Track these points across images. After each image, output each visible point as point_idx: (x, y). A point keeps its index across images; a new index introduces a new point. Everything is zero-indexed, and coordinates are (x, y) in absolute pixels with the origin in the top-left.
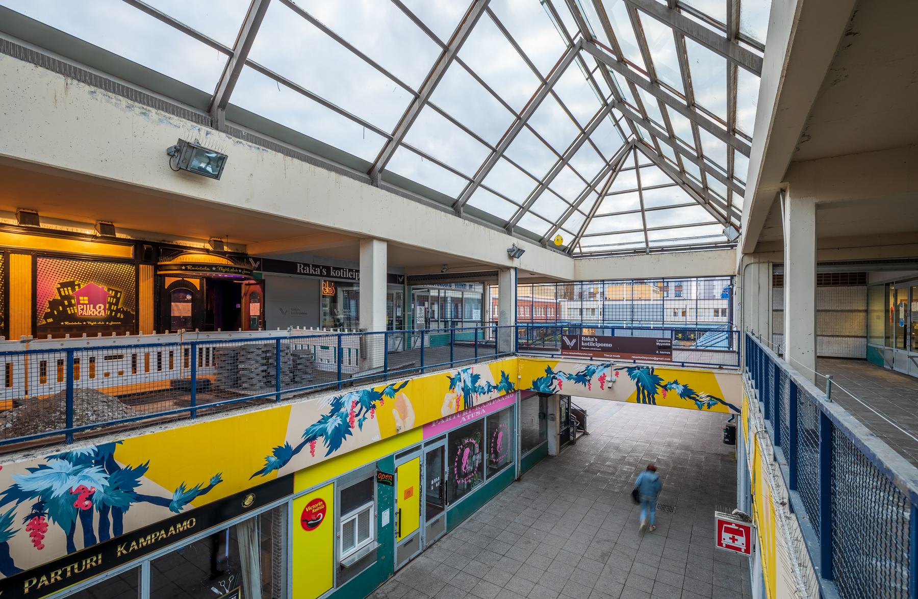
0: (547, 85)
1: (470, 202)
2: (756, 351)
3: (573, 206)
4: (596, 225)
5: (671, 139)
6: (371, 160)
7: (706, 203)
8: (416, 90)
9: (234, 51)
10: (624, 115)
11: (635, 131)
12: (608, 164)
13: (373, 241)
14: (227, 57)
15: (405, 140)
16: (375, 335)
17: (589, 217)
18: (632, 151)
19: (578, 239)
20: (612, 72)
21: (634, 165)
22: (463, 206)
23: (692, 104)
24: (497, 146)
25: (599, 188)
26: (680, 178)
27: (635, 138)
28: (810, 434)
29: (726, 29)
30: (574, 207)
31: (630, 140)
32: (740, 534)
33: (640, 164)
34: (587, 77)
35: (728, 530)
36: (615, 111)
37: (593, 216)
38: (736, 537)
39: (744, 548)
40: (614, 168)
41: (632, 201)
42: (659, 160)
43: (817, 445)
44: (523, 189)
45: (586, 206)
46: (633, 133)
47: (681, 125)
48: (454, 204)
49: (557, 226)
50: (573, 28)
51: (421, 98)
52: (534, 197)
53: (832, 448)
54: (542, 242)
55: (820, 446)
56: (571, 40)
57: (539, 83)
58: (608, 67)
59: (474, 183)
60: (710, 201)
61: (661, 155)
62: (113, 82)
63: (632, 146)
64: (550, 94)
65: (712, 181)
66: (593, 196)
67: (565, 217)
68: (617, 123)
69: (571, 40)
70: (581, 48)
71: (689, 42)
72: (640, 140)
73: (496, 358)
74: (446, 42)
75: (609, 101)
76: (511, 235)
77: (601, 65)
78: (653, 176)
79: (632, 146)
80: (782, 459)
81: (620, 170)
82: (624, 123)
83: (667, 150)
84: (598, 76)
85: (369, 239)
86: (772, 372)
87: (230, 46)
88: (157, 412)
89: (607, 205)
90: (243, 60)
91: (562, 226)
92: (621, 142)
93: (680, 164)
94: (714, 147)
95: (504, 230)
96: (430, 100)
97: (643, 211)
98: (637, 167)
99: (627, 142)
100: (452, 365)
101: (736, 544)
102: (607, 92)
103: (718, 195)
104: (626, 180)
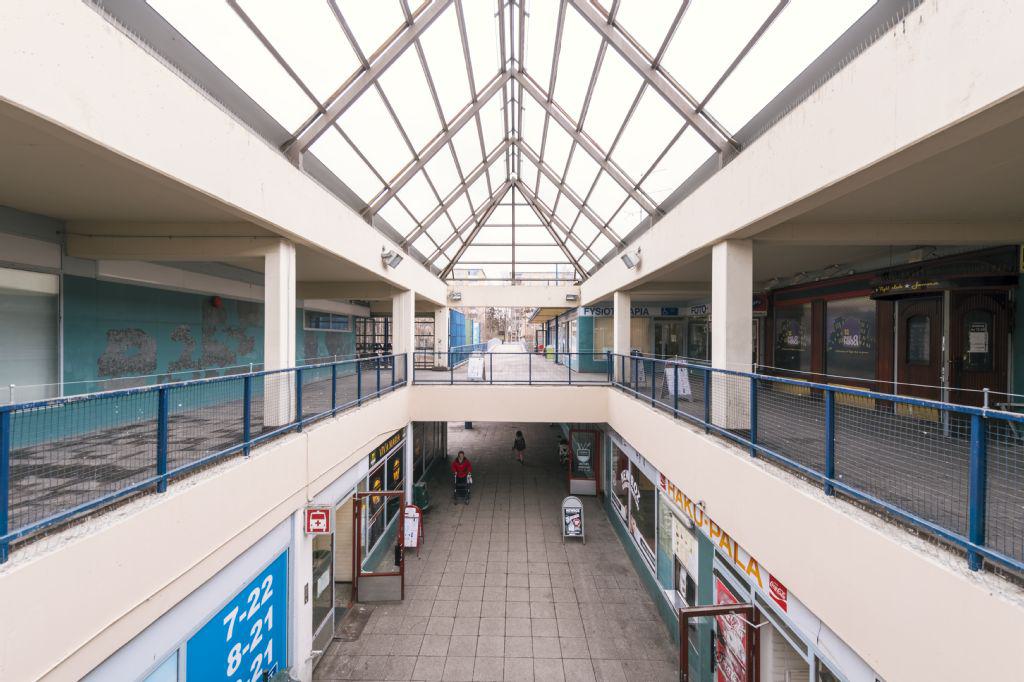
4: (471, 254)
6: (292, 130)
13: (277, 244)
25: (465, 236)
32: (321, 517)
35: (315, 517)
38: (320, 521)
39: (325, 528)
41: (505, 235)
45: (451, 252)
52: (672, 96)
64: (420, 172)
66: (458, 244)
71: (551, 119)
73: (393, 390)
85: (273, 236)
89: (484, 235)
91: (604, 172)
96: (338, 122)
99: (508, 180)
101: (321, 527)
104: (501, 214)
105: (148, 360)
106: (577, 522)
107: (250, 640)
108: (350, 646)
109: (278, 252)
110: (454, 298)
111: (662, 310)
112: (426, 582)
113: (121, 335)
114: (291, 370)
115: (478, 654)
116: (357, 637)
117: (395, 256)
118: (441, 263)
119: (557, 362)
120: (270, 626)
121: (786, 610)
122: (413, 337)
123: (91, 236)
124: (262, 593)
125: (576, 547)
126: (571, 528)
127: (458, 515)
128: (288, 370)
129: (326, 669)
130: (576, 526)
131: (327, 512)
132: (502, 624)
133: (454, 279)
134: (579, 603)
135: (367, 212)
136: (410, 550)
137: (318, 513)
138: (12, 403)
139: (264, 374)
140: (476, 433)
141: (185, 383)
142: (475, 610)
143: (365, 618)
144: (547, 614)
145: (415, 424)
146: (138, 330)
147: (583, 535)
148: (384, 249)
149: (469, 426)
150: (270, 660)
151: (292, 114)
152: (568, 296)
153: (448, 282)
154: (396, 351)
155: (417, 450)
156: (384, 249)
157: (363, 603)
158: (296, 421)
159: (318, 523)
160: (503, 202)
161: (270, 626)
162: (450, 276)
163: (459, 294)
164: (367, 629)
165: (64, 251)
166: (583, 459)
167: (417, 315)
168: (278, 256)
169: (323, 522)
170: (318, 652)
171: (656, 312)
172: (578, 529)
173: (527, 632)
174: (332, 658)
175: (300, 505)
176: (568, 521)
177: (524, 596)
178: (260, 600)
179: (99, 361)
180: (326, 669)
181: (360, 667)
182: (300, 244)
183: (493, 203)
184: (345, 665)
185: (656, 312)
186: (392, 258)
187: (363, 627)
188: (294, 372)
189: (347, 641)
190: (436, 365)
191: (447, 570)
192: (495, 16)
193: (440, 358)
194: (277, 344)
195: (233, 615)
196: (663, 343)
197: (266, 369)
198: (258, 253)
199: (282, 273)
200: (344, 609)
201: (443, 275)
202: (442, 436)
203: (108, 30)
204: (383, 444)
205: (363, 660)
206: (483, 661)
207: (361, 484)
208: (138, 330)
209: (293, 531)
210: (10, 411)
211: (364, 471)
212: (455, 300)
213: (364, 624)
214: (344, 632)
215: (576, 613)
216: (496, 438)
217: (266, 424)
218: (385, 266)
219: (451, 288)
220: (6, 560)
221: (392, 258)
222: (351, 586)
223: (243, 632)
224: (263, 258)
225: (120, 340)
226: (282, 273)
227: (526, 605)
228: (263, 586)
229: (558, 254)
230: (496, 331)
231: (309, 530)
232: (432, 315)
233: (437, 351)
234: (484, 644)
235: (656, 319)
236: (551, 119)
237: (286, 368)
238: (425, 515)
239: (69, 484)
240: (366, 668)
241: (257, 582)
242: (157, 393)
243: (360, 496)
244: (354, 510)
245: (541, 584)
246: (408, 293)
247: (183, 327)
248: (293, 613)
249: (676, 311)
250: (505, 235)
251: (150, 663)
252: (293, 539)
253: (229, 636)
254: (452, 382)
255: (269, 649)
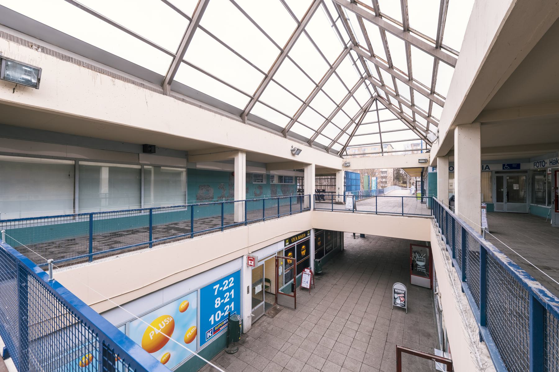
0: (333, 69)
1: (316, 140)
2: (439, 209)
3: (343, 131)
4: (355, 141)
5: (397, 96)
7: (414, 129)
8: (266, 72)
9: (176, 54)
10: (371, 83)
11: (376, 90)
12: (362, 108)
14: (172, 58)
15: (260, 99)
16: (239, 202)
17: (351, 136)
18: (375, 101)
19: (345, 148)
20: (366, 61)
21: (376, 109)
22: (247, 115)
23: (411, 79)
24: (306, 101)
25: (357, 121)
26: (401, 116)
27: (377, 95)
28: (472, 254)
29: (402, 26)
30: (343, 131)
31: (374, 96)
33: (379, 108)
34: (353, 63)
35: (250, 260)
36: (366, 81)
37: (353, 136)
38: (252, 262)
40: (365, 111)
41: (375, 128)
42: (389, 106)
43: (479, 262)
44: (317, 122)
45: (350, 131)
46: (375, 92)
47: (404, 90)
48: (283, 131)
49: (334, 141)
50: (347, 38)
51: (268, 77)
52: (324, 126)
53: (486, 262)
54: (310, 142)
55: (480, 262)
56: (346, 45)
57: (329, 67)
58: (365, 59)
59: (294, 120)
60: (417, 128)
61: (390, 104)
62: (115, 74)
63: (375, 99)
64: (334, 74)
65: (418, 118)
66: (354, 125)
67: (340, 136)
68: (367, 87)
69: (346, 45)
70: (351, 49)
71: (413, 48)
72: (379, 96)
74: (282, 47)
75: (364, 76)
76: (245, 123)
77: (361, 57)
78: (386, 114)
79: (375, 99)
80: (457, 266)
81: (368, 111)
82: (371, 87)
83: (394, 102)
84: (359, 63)
85: (236, 151)
86: (450, 221)
87: (174, 52)
88: (123, 246)
89: (361, 129)
90: (181, 60)
92: (369, 96)
93: (401, 109)
94: (422, 102)
95: (326, 151)
97: (380, 133)
98: (377, 110)
99: (372, 97)
100: (279, 216)
102: (362, 71)
103: (368, 101)
104: (371, 117)
105: (211, 196)
106: (402, 299)
107: (224, 298)
108: (269, 320)
109: (238, 156)
110: (346, 165)
111: (504, 165)
112: (309, 305)
113: (203, 187)
114: (244, 201)
115: (320, 343)
116: (273, 317)
117: (296, 149)
118: (337, 147)
119: (422, 201)
120: (233, 297)
121: (249, 286)
122: (343, 187)
123: (193, 155)
124: (229, 283)
125: (400, 313)
126: (398, 301)
127: (337, 280)
128: (243, 201)
129: (258, 324)
130: (401, 301)
131: (254, 258)
132: (337, 335)
133: (347, 155)
134: (386, 341)
135: (284, 132)
136: (304, 289)
137: (251, 258)
138: (153, 207)
139: (234, 202)
140: (366, 240)
141: (199, 204)
142: (326, 325)
143: (277, 311)
144: (364, 340)
145: (316, 230)
146: (208, 185)
147: (406, 307)
148: (292, 147)
149: (362, 236)
150: (233, 309)
151: (241, 103)
152: (419, 160)
153: (343, 157)
154: (306, 193)
155: (319, 243)
156: (292, 147)
157: (279, 305)
158: (245, 221)
159: (251, 263)
160: (370, 109)
161: (233, 297)
162: (345, 153)
163: (349, 163)
164: (277, 316)
165: (188, 161)
166: (421, 264)
167: (316, 175)
168: (238, 157)
169: (253, 262)
170: (253, 315)
171: (500, 168)
172: (402, 303)
173: (349, 344)
174: (261, 321)
175: (245, 253)
176: (396, 297)
177: (355, 327)
178: (228, 285)
179: (197, 196)
180: (258, 324)
181: (270, 329)
182: (247, 152)
183: (365, 111)
184: (265, 326)
185: (500, 168)
186: (295, 151)
187: (277, 314)
188: (244, 202)
189: (268, 317)
190: (337, 201)
191: (321, 303)
192: (332, 26)
193: (339, 197)
194: (238, 191)
195: (217, 286)
196: (504, 190)
197: (235, 200)
198: (232, 157)
199: (240, 163)
200: (271, 305)
201: (340, 154)
202: (340, 238)
203: (175, 101)
204: (294, 237)
205: (272, 326)
206: (321, 347)
207: (279, 252)
208: (208, 185)
209: (242, 263)
210: (152, 209)
211: (281, 246)
212: (347, 166)
213: (277, 313)
214: (269, 313)
215: (383, 346)
216: (377, 244)
217: (235, 221)
218: (293, 155)
219: (345, 160)
220: (152, 248)
221: (295, 151)
222: (274, 296)
223: (221, 294)
224: (234, 158)
225: (202, 189)
226: (240, 163)
227: (355, 332)
228: (230, 281)
229: (411, 134)
230: (402, 182)
231: (248, 265)
232: (335, 175)
233: (337, 194)
234: (324, 341)
235: (497, 172)
236: (413, 48)
237: (241, 200)
238: (317, 275)
239: (177, 233)
240: (272, 330)
241: (227, 278)
242: (191, 207)
243: (278, 257)
244: (276, 263)
245: (368, 325)
246: (311, 166)
247: (222, 184)
248: (243, 295)
249: (518, 166)
250: (375, 128)
251: (187, 291)
252: (242, 267)
253: (216, 294)
254: (403, 214)
255: (232, 305)
